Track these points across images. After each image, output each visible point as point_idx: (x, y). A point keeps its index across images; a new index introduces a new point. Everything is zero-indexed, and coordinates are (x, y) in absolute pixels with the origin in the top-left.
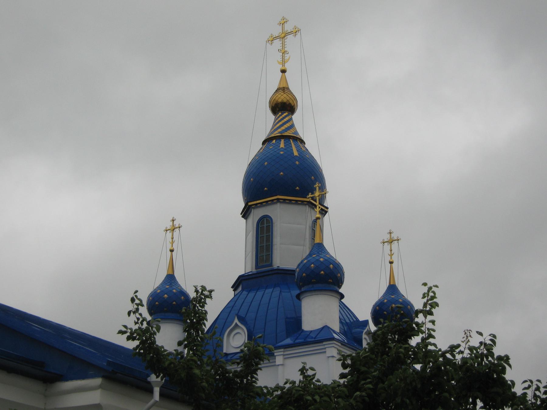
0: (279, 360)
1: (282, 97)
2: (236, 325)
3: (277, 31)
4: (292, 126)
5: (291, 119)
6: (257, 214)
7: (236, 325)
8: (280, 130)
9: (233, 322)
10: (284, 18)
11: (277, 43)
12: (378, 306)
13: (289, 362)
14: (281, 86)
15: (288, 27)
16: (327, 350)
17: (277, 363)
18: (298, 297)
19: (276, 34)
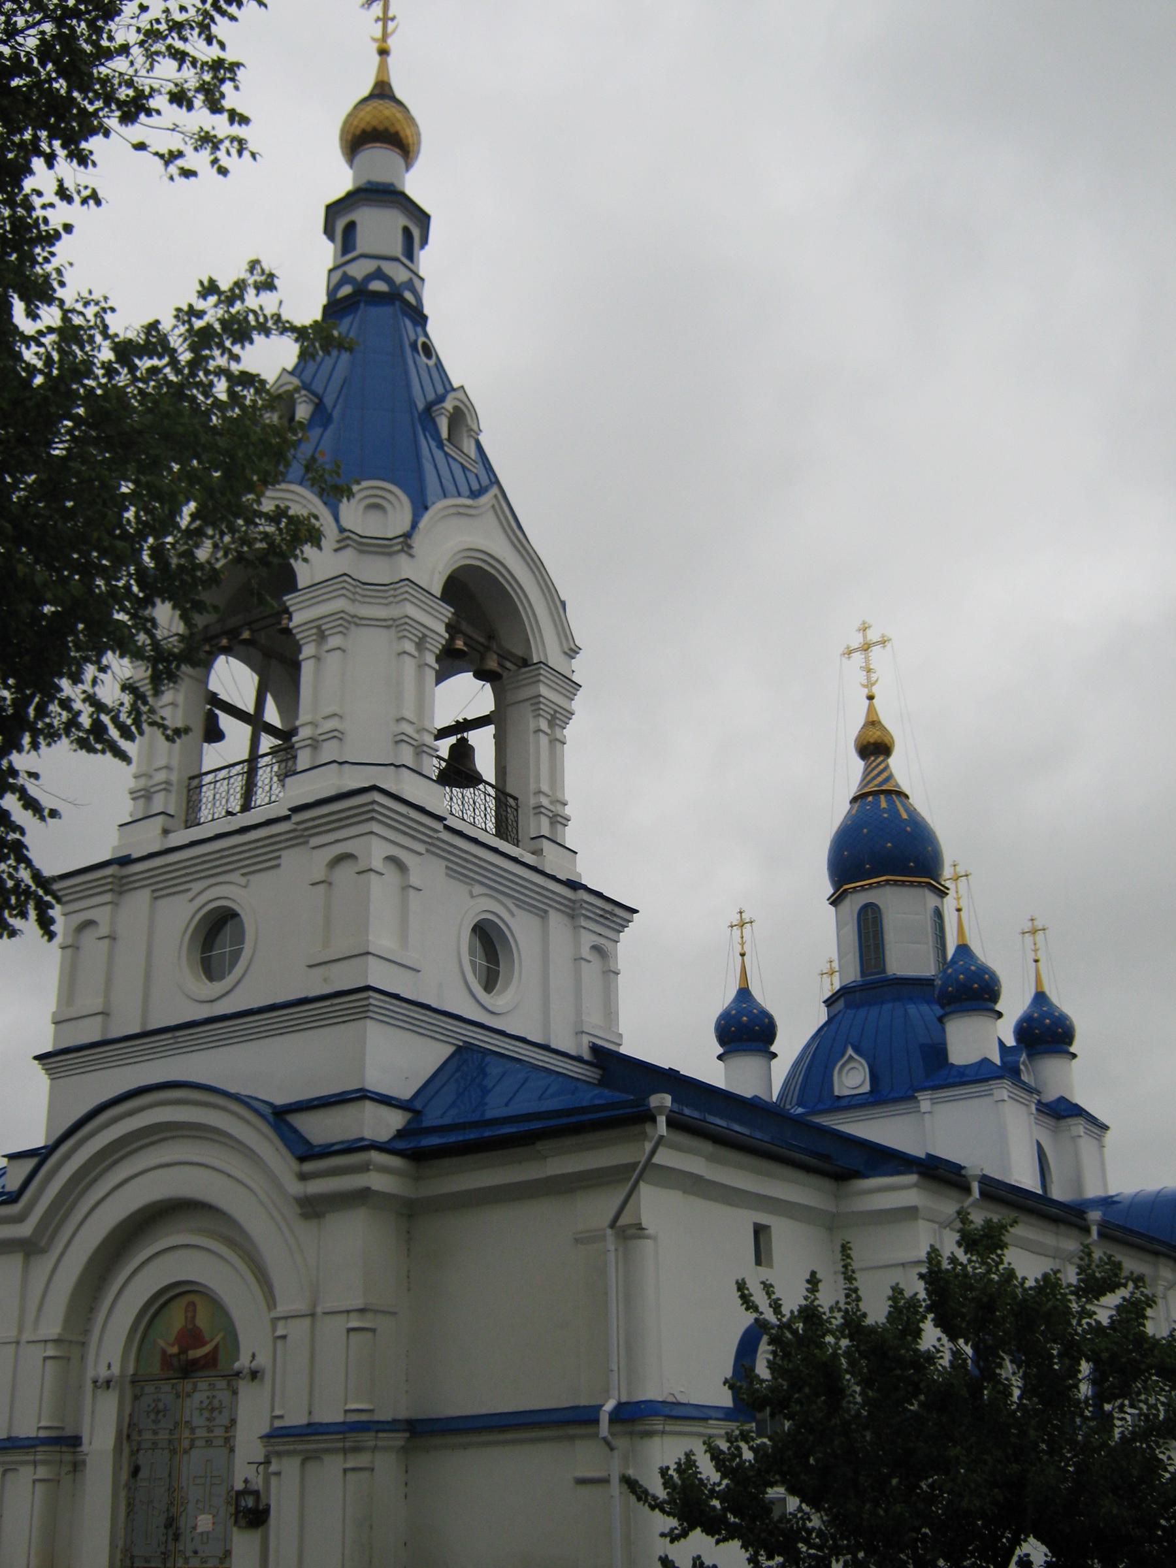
0: (925, 1105)
1: (874, 735)
2: (851, 1057)
3: (856, 640)
4: (890, 777)
5: (887, 767)
6: (854, 903)
7: (851, 1057)
8: (875, 782)
9: (843, 1055)
10: (864, 623)
11: (858, 657)
12: (723, 1019)
13: (939, 1107)
14: (871, 720)
15: (873, 635)
16: (995, 1091)
17: (923, 1110)
18: (941, 1020)
19: (855, 645)
